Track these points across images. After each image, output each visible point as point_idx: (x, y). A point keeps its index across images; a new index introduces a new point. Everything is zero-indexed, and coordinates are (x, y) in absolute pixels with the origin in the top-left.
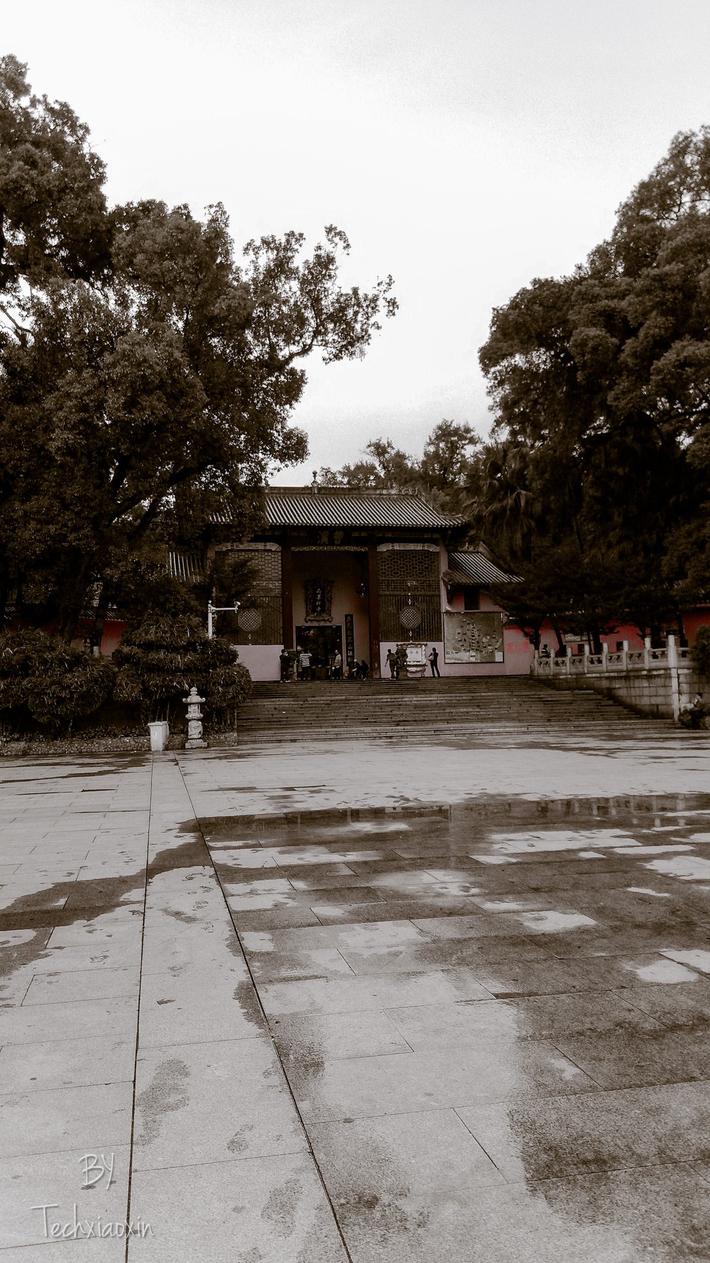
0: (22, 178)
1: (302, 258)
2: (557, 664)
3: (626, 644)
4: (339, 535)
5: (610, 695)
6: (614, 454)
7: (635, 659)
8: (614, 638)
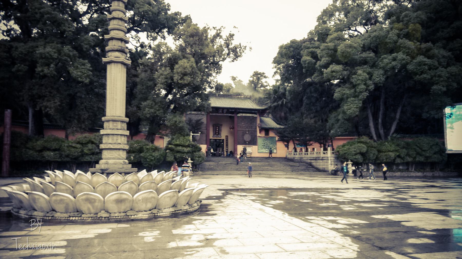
1: (225, 34)
2: (294, 154)
3: (315, 149)
4: (225, 111)
5: (310, 164)
6: (313, 89)
7: (318, 154)
8: (312, 147)
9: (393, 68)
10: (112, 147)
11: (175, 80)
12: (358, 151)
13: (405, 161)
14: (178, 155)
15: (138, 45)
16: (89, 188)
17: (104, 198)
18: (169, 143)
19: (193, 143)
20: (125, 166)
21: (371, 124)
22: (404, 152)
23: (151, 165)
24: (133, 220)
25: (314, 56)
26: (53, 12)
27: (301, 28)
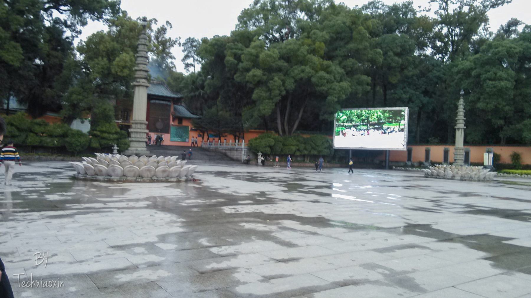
5: (225, 155)
9: (301, 79)
12: (268, 144)
13: (303, 153)
14: (104, 142)
21: (279, 121)
22: (302, 146)
25: (238, 58)
27: (225, 27)
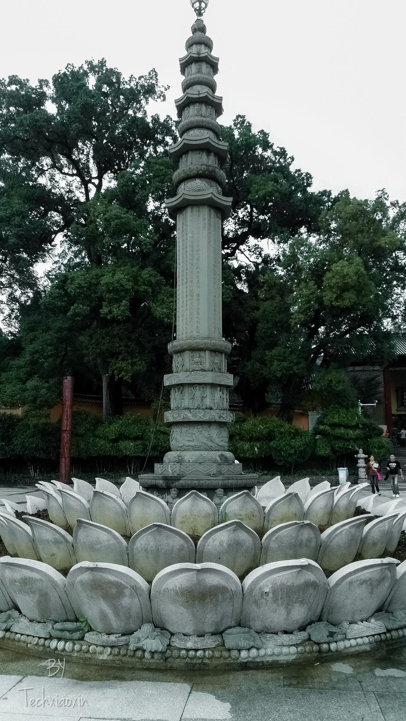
0: (274, 190)
10: (191, 417)
11: (326, 303)
14: (339, 444)
15: (260, 260)
16: (112, 541)
17: (150, 582)
18: (320, 422)
19: (365, 420)
20: (225, 468)
23: (290, 463)
24: (246, 667)
26: (122, 215)
